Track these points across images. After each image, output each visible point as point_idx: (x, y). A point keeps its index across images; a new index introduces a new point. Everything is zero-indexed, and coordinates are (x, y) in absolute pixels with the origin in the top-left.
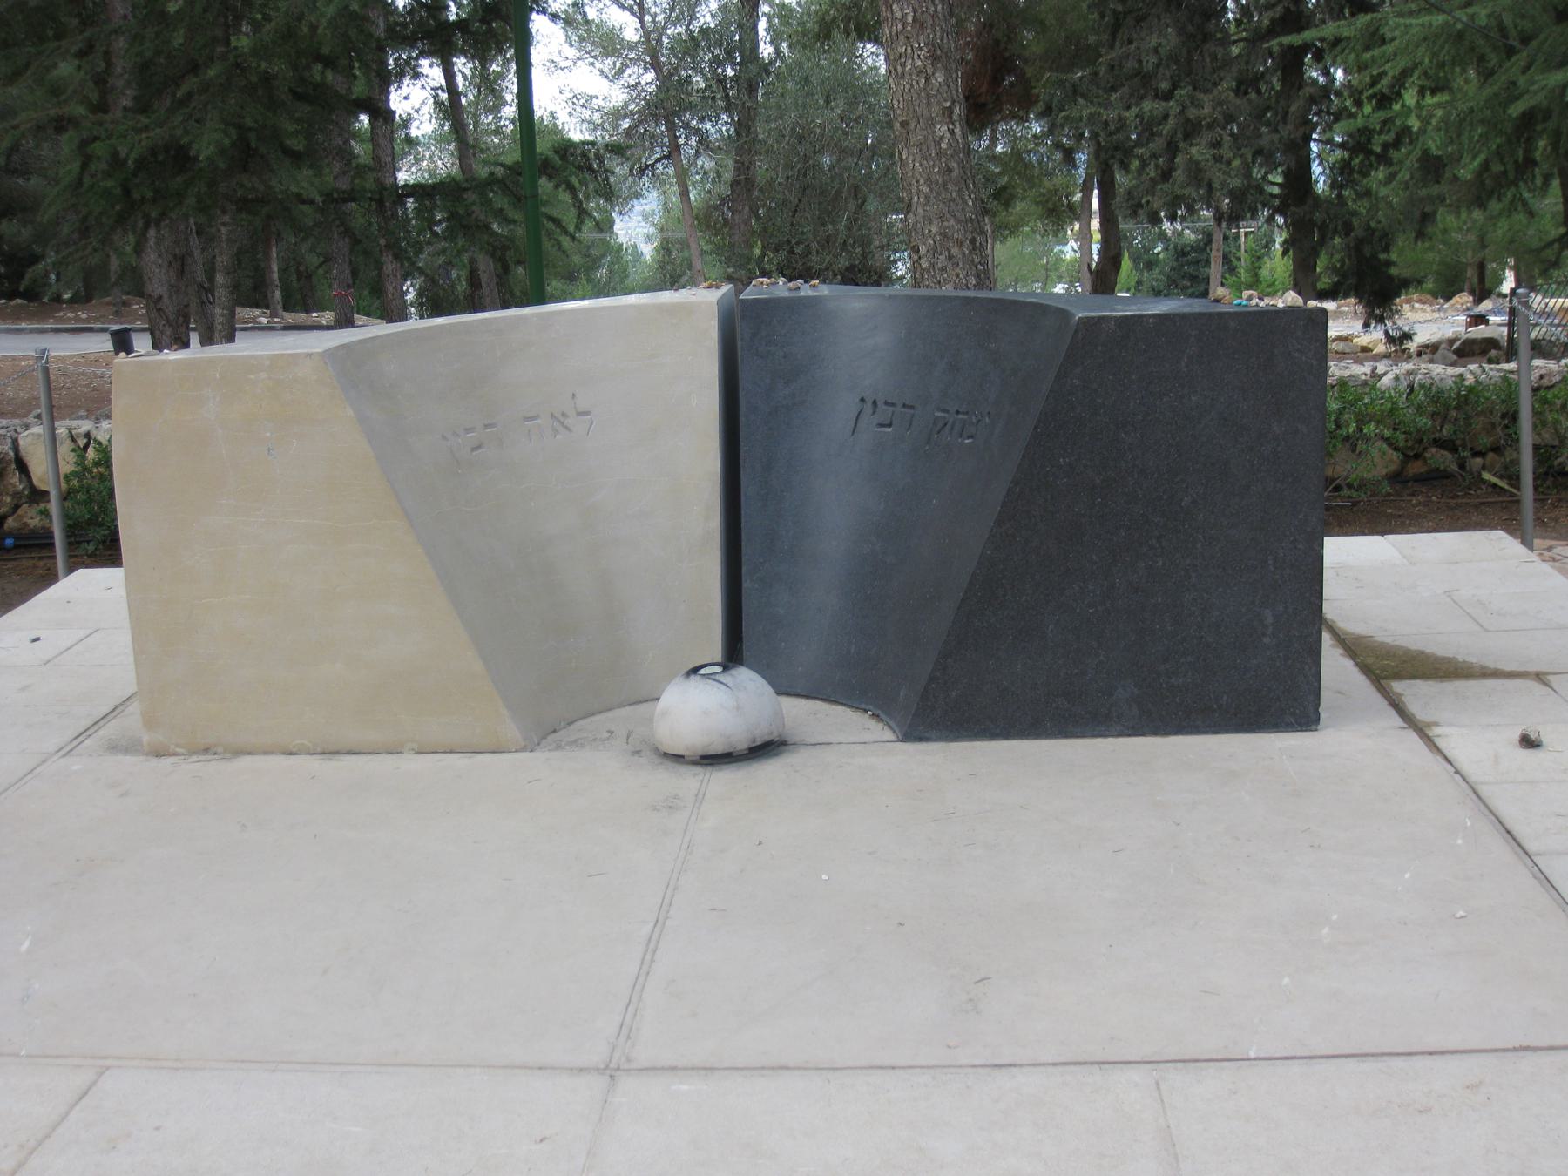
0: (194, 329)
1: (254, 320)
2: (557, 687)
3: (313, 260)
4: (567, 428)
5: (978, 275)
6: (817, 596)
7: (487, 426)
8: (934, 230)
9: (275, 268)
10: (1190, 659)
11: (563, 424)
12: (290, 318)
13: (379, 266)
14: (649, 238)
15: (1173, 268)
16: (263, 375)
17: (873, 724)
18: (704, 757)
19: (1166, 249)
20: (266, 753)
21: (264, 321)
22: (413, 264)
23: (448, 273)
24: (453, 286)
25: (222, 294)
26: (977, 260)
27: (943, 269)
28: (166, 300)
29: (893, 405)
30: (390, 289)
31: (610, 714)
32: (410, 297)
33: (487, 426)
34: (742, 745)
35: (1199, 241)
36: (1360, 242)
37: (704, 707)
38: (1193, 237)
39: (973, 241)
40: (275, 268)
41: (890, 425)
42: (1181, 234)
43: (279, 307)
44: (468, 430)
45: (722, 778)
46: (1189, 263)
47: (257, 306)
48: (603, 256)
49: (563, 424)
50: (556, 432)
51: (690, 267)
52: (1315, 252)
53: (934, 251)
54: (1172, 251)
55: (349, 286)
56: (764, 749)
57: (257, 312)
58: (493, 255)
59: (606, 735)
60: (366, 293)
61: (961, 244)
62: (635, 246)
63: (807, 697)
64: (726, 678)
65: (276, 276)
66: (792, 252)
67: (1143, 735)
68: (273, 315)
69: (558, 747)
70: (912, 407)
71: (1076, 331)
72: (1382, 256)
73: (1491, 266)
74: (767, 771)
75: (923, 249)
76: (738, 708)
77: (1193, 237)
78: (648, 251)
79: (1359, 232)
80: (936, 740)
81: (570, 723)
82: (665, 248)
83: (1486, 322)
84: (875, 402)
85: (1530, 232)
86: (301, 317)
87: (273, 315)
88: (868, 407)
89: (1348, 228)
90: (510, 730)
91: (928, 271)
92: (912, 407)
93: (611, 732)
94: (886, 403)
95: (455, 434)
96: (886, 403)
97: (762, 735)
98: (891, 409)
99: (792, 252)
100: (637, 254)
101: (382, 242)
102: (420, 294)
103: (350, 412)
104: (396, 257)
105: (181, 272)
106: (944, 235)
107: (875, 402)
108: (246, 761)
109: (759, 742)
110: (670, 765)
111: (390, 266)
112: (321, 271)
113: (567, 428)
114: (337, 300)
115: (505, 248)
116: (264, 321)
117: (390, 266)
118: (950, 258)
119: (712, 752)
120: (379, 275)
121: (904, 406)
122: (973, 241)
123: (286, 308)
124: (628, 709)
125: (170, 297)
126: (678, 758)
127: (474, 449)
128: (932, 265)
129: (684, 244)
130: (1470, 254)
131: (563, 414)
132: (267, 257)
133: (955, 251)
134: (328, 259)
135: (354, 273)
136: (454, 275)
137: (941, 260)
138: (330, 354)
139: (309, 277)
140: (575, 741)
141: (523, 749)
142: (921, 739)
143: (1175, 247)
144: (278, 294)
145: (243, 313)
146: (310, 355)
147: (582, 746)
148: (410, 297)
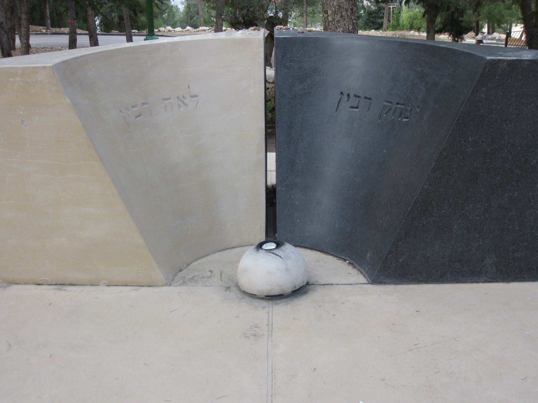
0: (17, 34)
1: (40, 31)
2: (180, 247)
3: (62, 9)
4: (186, 105)
5: (353, 24)
6: (324, 203)
7: (143, 104)
8: (335, 4)
9: (48, 11)
10: (525, 244)
11: (183, 102)
12: (54, 30)
13: (86, 12)
14: (182, 3)
15: (367, 19)
16: (18, 79)
17: (350, 269)
18: (266, 296)
19: (364, 12)
20: (25, 284)
21: (44, 31)
22: (99, 12)
23: (111, 15)
24: (113, 19)
25: (24, 22)
26: (353, 18)
27: (338, 21)
28: (4, 23)
29: (359, 97)
30: (90, 20)
31: (208, 258)
32: (97, 22)
33: (143, 104)
34: (289, 290)
35: (376, 10)
36: (453, 13)
37: (266, 268)
38: (374, 8)
39: (352, 9)
40: (48, 11)
41: (357, 108)
42: (370, 7)
43: (50, 26)
44: (133, 107)
45: (280, 309)
46: (372, 17)
47: (41, 25)
48: (166, 9)
49: (183, 102)
50: (180, 106)
51: (198, 14)
52: (435, 16)
53: (335, 13)
54: (366, 13)
55: (75, 19)
56: (299, 291)
57: (42, 28)
58: (130, 9)
59: (209, 274)
60: (81, 21)
61: (347, 11)
62: (177, 6)
63: (311, 249)
64: (276, 252)
65: (48, 15)
66: (248, 10)
67: (497, 282)
68: (47, 29)
69: (184, 283)
70: (370, 99)
71: (485, 68)
72: (460, 19)
73: (480, 23)
74: (302, 304)
75: (330, 12)
76: (287, 270)
77: (374, 8)
78: (181, 8)
79: (452, 9)
80: (389, 284)
81: (188, 265)
82: (188, 7)
83: (483, 42)
84: (348, 95)
85: (496, 11)
86: (58, 30)
87: (47, 29)
88: (345, 97)
89: (448, 9)
90: (158, 275)
91: (331, 22)
92: (370, 99)
93: (211, 272)
94: (355, 96)
95: (127, 109)
96: (355, 96)
97: (299, 282)
98: (358, 99)
99: (248, 10)
100: (178, 9)
101: (87, 3)
102: (101, 22)
103: (68, 101)
104: (93, 9)
105: (12, 13)
106: (340, 6)
107: (348, 95)
108: (15, 288)
109: (297, 288)
110: (248, 299)
111: (90, 12)
112: (65, 13)
113: (186, 105)
114: (70, 25)
115: (135, 6)
116: (44, 31)
117: (90, 12)
118: (342, 16)
119: (272, 295)
120: (86, 15)
121: (365, 98)
122: (352, 9)
123: (52, 27)
124: (218, 254)
125: (6, 23)
126: (253, 296)
127: (137, 117)
128: (334, 19)
129: (195, 6)
130: (474, 18)
131: (183, 97)
132: (45, 8)
133: (344, 13)
134: (67, 9)
135: (77, 14)
136: (113, 15)
137: (338, 17)
138: (58, 67)
139: (60, 15)
140: (193, 278)
141: (166, 285)
142: (381, 283)
143: (368, 11)
144: (49, 21)
145: (32, 28)
146: (45, 68)
147: (197, 282)
148: (97, 22)
